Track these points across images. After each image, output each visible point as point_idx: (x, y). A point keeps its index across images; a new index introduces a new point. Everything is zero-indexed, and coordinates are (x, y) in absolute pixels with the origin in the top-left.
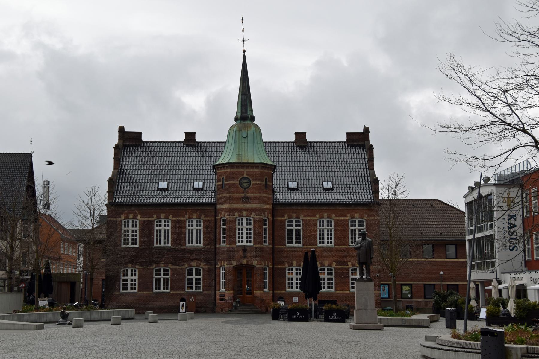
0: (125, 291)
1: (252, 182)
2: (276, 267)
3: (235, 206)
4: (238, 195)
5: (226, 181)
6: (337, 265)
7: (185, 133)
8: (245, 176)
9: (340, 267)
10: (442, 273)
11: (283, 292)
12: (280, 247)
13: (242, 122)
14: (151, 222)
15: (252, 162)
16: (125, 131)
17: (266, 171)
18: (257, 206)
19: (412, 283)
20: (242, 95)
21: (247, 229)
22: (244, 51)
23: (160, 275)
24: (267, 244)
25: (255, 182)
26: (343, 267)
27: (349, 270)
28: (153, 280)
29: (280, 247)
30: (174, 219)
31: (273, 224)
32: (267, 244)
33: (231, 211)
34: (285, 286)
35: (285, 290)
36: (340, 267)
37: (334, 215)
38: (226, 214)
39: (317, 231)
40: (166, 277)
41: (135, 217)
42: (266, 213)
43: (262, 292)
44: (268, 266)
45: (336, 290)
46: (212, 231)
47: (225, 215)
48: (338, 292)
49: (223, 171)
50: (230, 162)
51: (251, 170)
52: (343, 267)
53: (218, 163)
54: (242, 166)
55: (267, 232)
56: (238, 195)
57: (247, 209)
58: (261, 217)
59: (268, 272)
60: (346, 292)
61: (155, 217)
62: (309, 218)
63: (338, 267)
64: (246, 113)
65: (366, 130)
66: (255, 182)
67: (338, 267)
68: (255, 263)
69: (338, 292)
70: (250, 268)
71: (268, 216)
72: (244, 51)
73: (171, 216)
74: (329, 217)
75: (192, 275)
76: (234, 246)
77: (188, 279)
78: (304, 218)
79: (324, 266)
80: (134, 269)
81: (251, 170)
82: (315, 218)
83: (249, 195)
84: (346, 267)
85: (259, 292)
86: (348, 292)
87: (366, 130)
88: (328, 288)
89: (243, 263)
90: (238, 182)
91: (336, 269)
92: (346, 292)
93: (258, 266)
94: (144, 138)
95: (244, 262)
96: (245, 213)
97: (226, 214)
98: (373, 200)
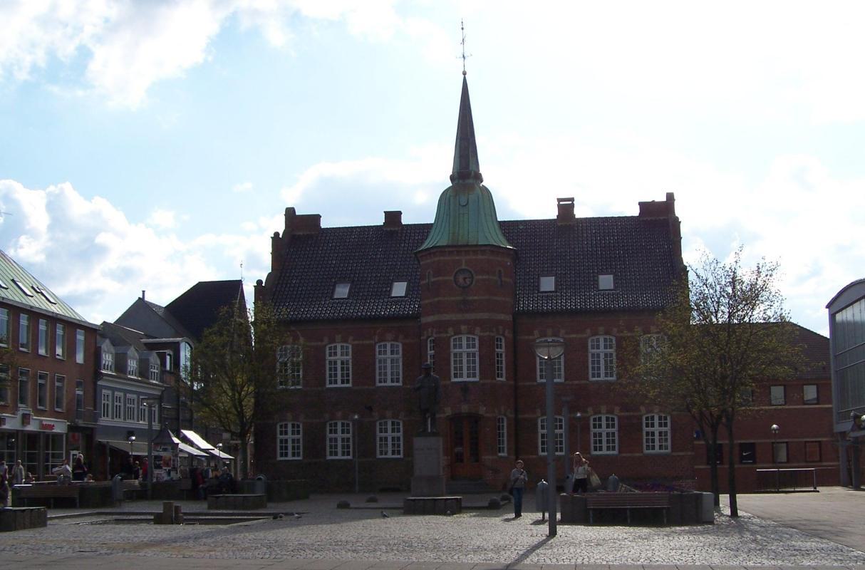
0: (383, 456)
1: (476, 277)
2: (520, 416)
3: (447, 317)
4: (453, 298)
5: (434, 277)
6: (621, 410)
7: (385, 212)
8: (463, 267)
9: (627, 414)
10: (775, 426)
11: (534, 456)
12: (527, 384)
13: (461, 181)
14: (322, 350)
15: (475, 243)
16: (297, 214)
17: (499, 259)
18: (485, 316)
19: (820, 439)
20: (461, 140)
21: (468, 355)
22: (464, 74)
23: (336, 432)
24: (503, 379)
25: (480, 277)
26: (632, 414)
27: (641, 419)
28: (375, 439)
29: (527, 384)
30: (356, 342)
31: (514, 347)
32: (503, 379)
33: (442, 326)
34: (537, 447)
35: (537, 454)
36: (627, 414)
37: (615, 330)
38: (435, 330)
39: (587, 356)
40: (396, 434)
41: (296, 338)
42: (501, 327)
43: (495, 457)
44: (505, 415)
45: (620, 452)
46: (413, 358)
47: (432, 333)
48: (624, 455)
49: (428, 261)
50: (438, 245)
51: (474, 257)
52: (632, 414)
53: (424, 247)
54: (458, 252)
55: (504, 359)
56: (453, 298)
57: (466, 322)
58: (492, 334)
59: (505, 424)
60: (637, 455)
61: (326, 340)
62: (574, 336)
63: (623, 414)
64: (468, 165)
65: (670, 197)
66: (480, 277)
67: (623, 414)
68: (482, 410)
69: (624, 455)
70: (475, 419)
71: (504, 332)
72: (464, 74)
73: (351, 338)
74: (607, 333)
75: (386, 432)
76: (448, 382)
77: (281, 441)
78: (566, 336)
79: (600, 413)
80: (296, 423)
81: (474, 257)
82: (585, 336)
83: (470, 298)
84: (636, 414)
85: (490, 457)
86: (641, 455)
87: (670, 197)
88: (608, 448)
89: (463, 411)
90: (452, 278)
91: (620, 418)
92: (637, 455)
93: (488, 415)
94: (324, 224)
95: (465, 408)
96: (463, 328)
97: (435, 330)
98: (724, 499)
